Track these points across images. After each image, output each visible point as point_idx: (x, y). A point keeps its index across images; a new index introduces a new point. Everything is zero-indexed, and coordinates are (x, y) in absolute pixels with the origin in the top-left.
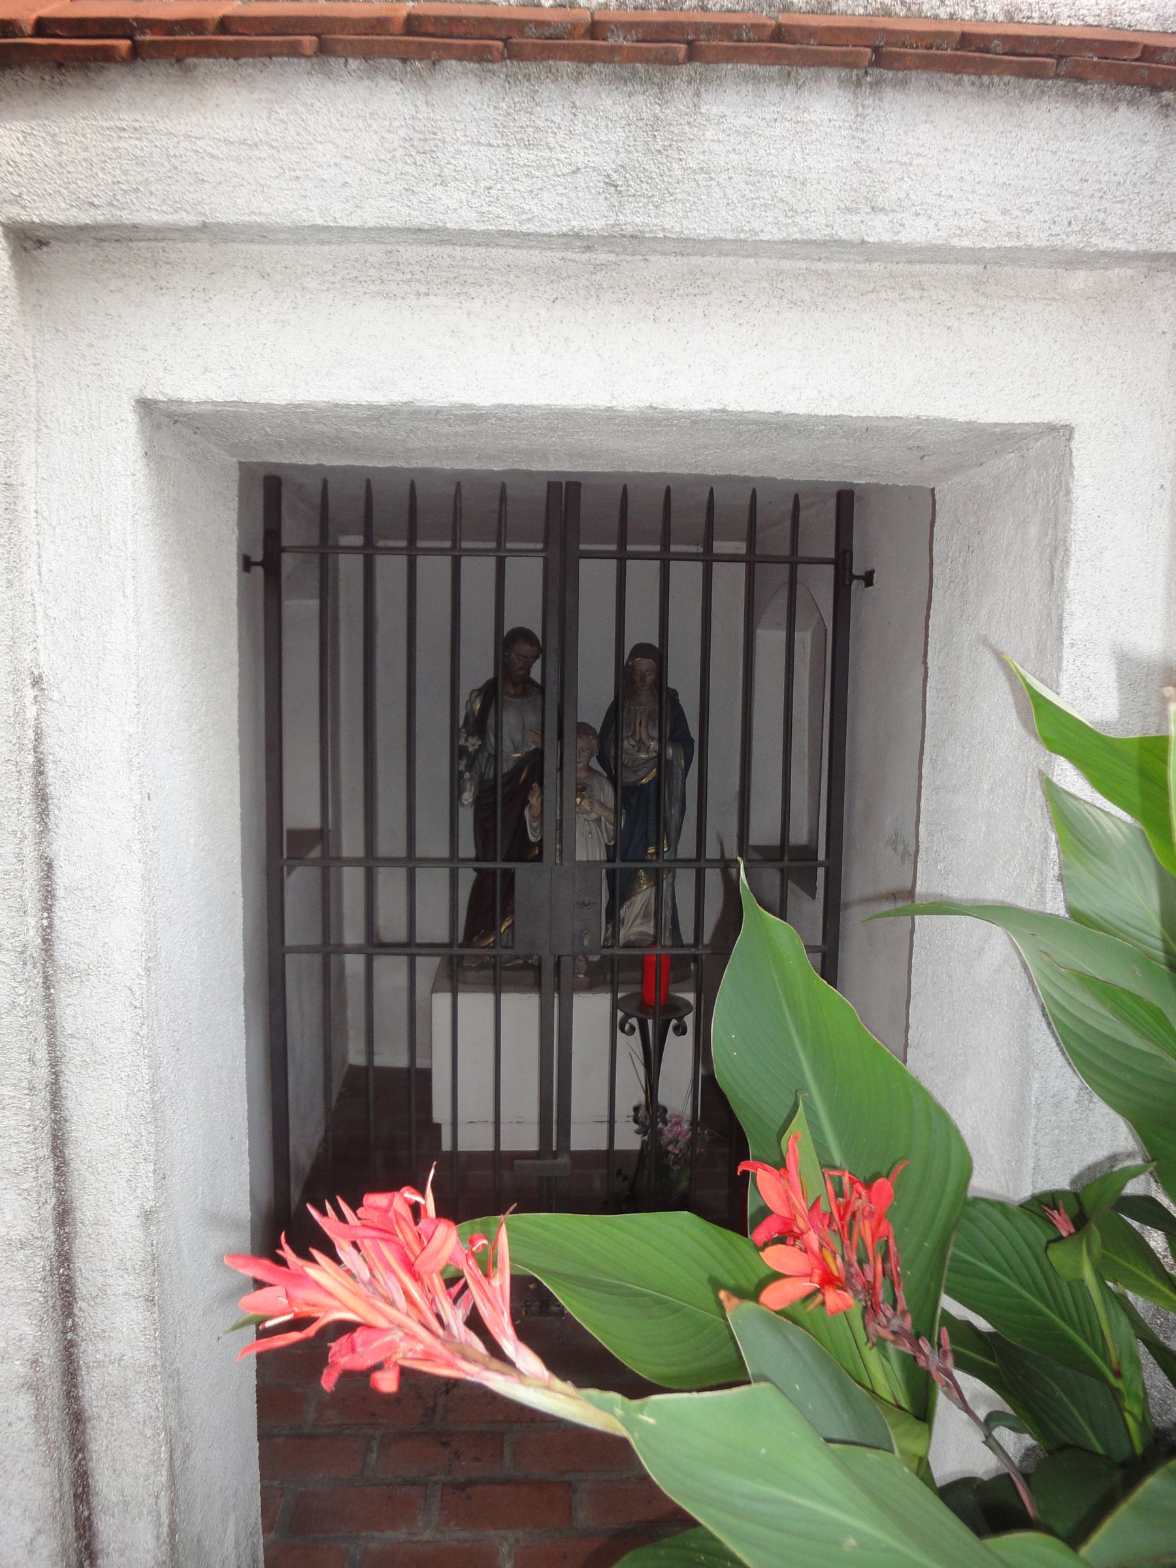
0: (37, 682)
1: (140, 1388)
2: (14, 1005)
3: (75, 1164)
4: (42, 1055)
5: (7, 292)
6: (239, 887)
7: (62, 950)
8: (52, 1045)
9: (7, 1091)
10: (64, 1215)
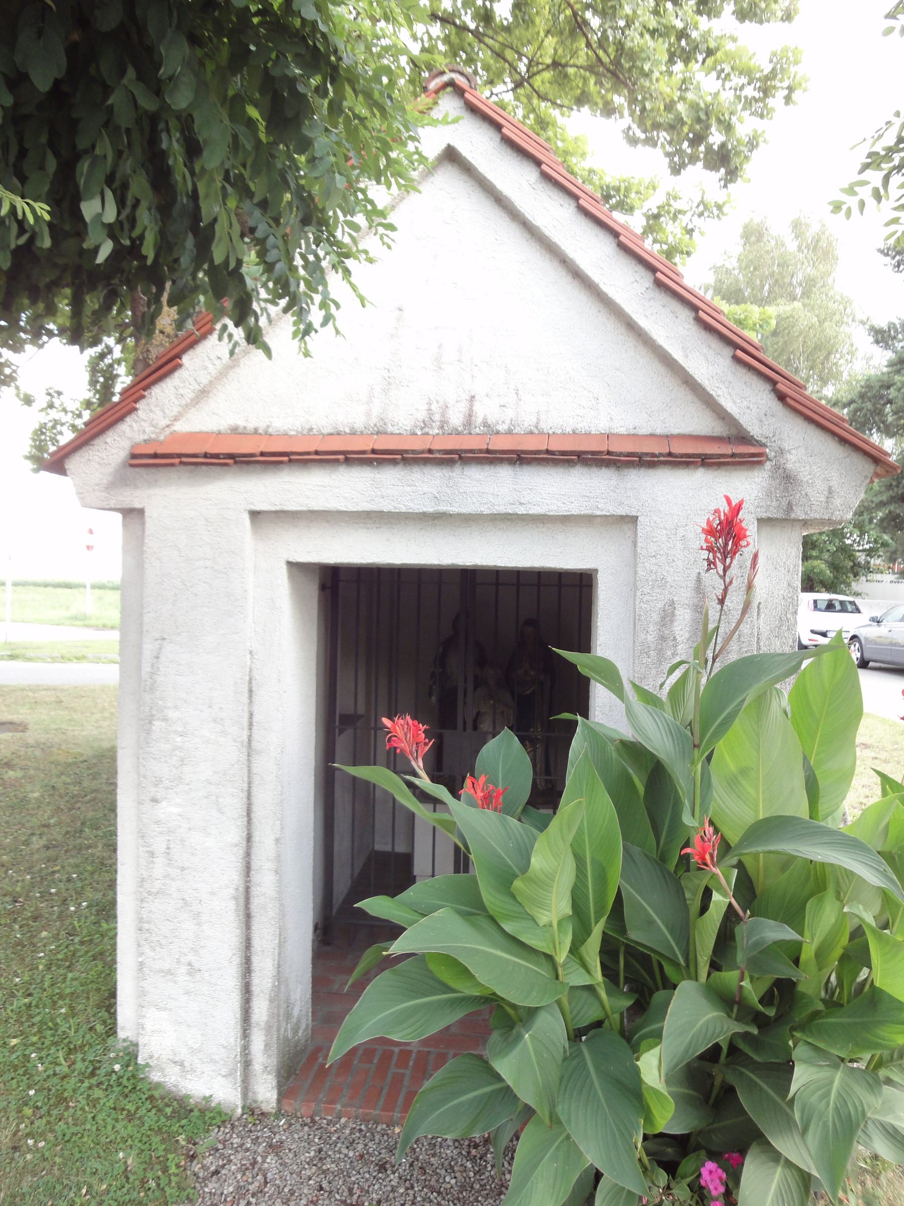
0: (251, 653)
1: (271, 905)
2: (239, 761)
3: (254, 820)
4: (246, 779)
5: (217, 362)
6: (314, 729)
7: (255, 744)
8: (249, 777)
9: (50, 1203)
10: (249, 838)
